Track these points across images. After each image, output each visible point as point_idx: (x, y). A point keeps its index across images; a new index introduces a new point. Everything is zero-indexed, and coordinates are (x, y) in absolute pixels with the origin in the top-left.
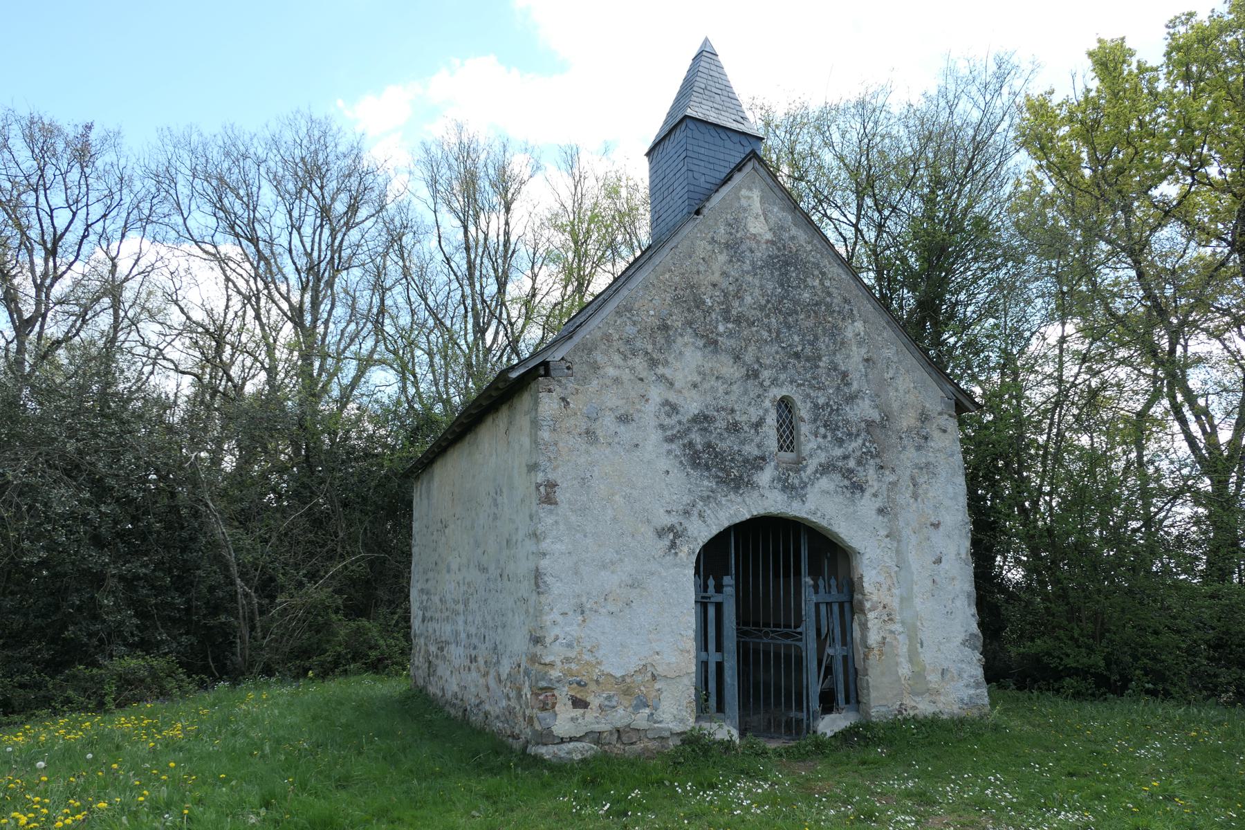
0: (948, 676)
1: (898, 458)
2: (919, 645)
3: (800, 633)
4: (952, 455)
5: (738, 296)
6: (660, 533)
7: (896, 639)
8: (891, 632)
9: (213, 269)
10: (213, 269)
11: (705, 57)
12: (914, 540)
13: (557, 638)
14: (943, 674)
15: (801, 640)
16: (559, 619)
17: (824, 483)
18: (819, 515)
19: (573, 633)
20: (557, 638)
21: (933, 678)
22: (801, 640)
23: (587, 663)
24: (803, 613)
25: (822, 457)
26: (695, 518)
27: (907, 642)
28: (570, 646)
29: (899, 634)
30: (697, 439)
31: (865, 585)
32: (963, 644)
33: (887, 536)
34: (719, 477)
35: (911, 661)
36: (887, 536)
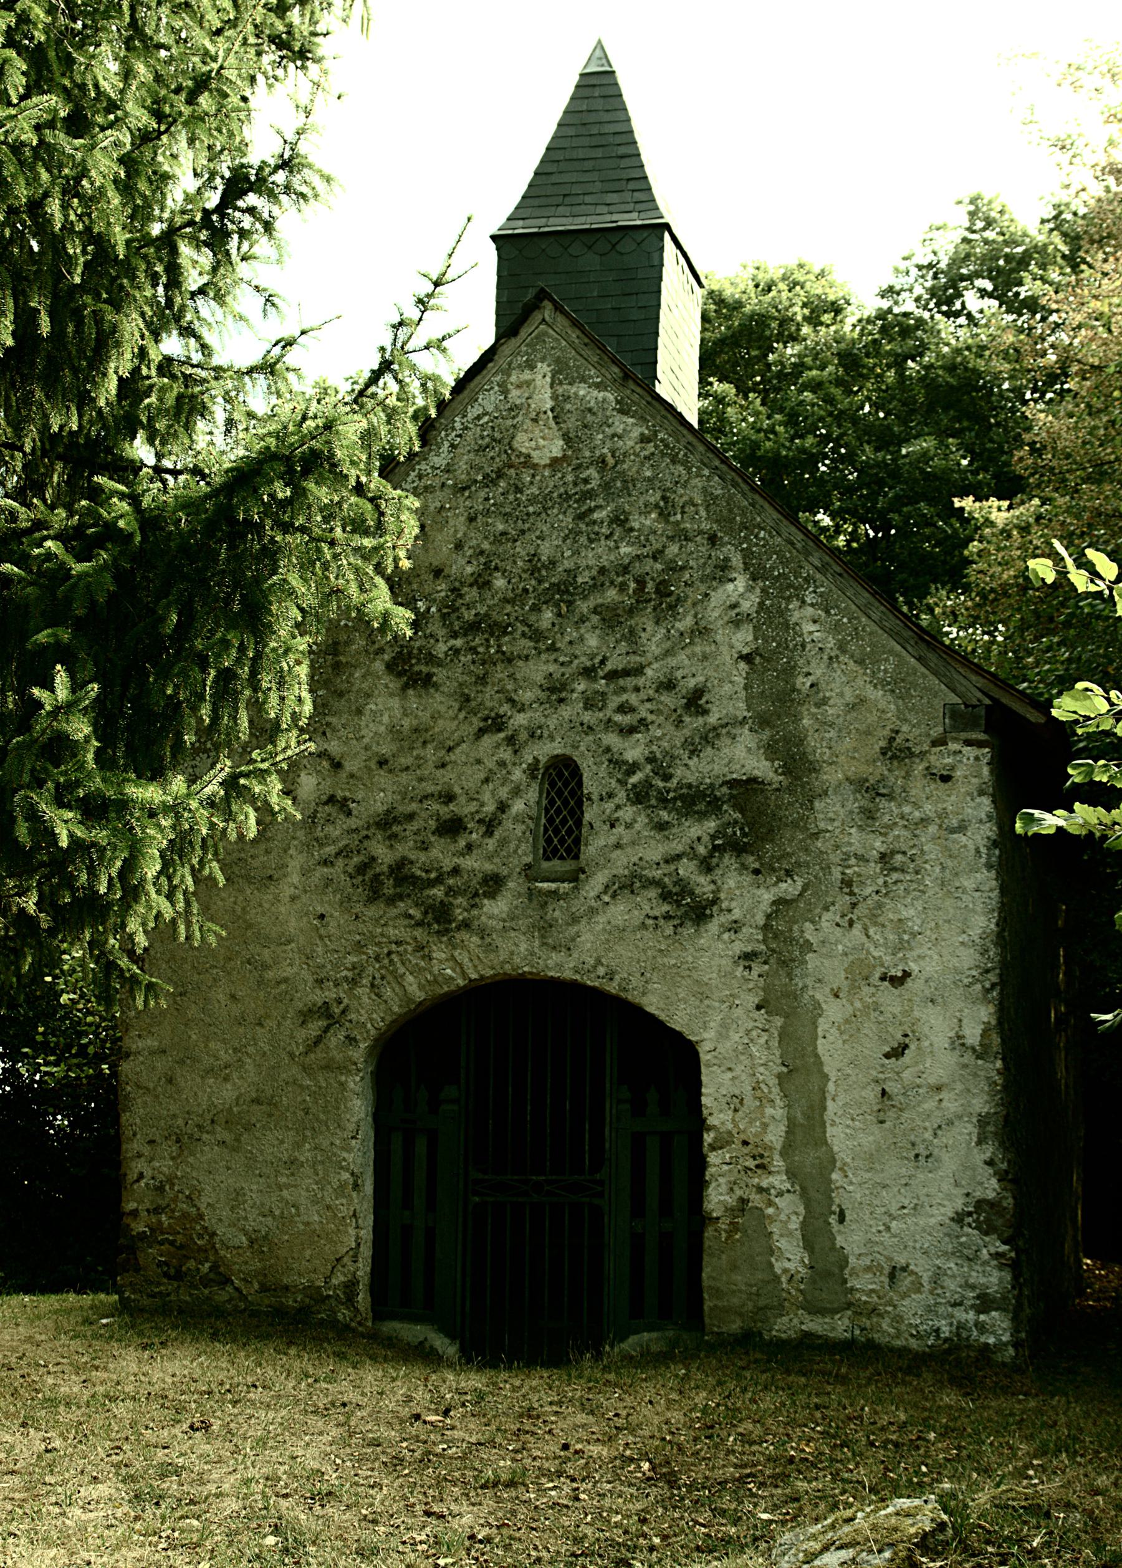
0: (907, 1281)
1: (807, 850)
2: (833, 1220)
3: (601, 1183)
4: (962, 828)
5: (482, 582)
6: (306, 1015)
7: (770, 1204)
8: (761, 1190)
9: (905, 259)
10: (905, 259)
11: (600, 45)
12: (834, 1011)
13: (141, 1176)
14: (892, 1276)
15: (601, 1195)
16: (146, 1150)
17: (619, 912)
18: (601, 971)
19: (165, 1169)
20: (141, 1176)
21: (864, 1284)
22: (601, 1195)
23: (185, 1215)
24: (607, 1145)
25: (621, 863)
26: (363, 991)
27: (801, 1210)
28: (160, 1189)
29: (780, 1194)
30: (384, 854)
31: (704, 1100)
32: (959, 1218)
33: (759, 1007)
34: (410, 917)
35: (808, 1245)
36: (759, 1007)
